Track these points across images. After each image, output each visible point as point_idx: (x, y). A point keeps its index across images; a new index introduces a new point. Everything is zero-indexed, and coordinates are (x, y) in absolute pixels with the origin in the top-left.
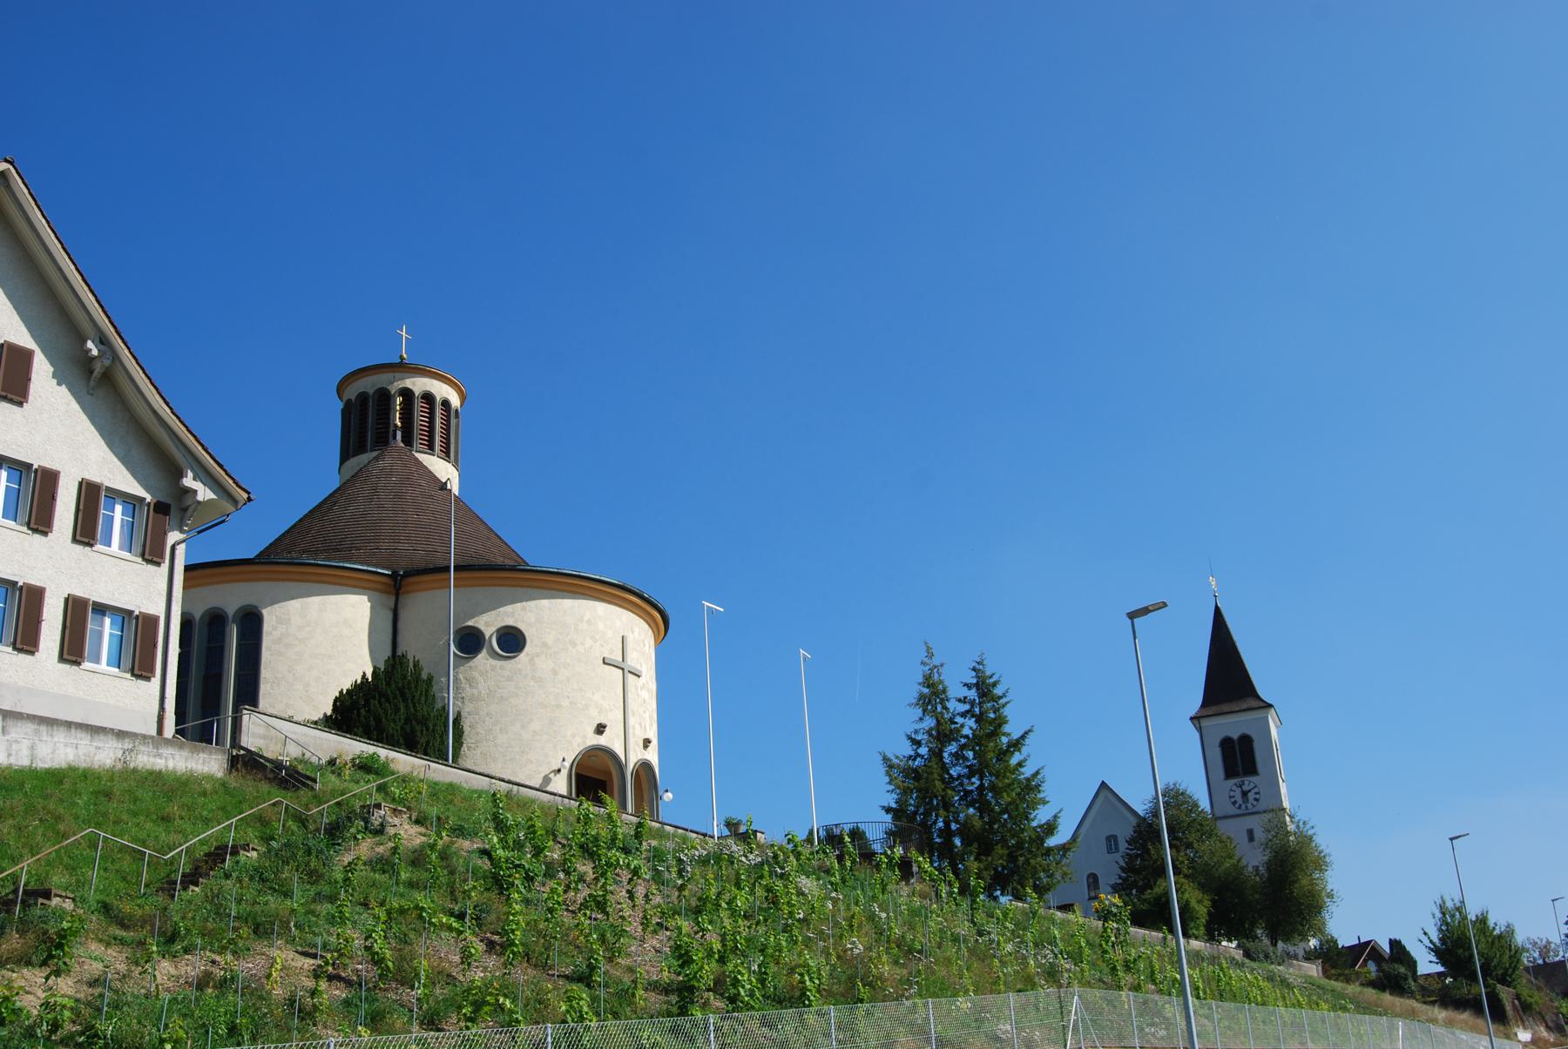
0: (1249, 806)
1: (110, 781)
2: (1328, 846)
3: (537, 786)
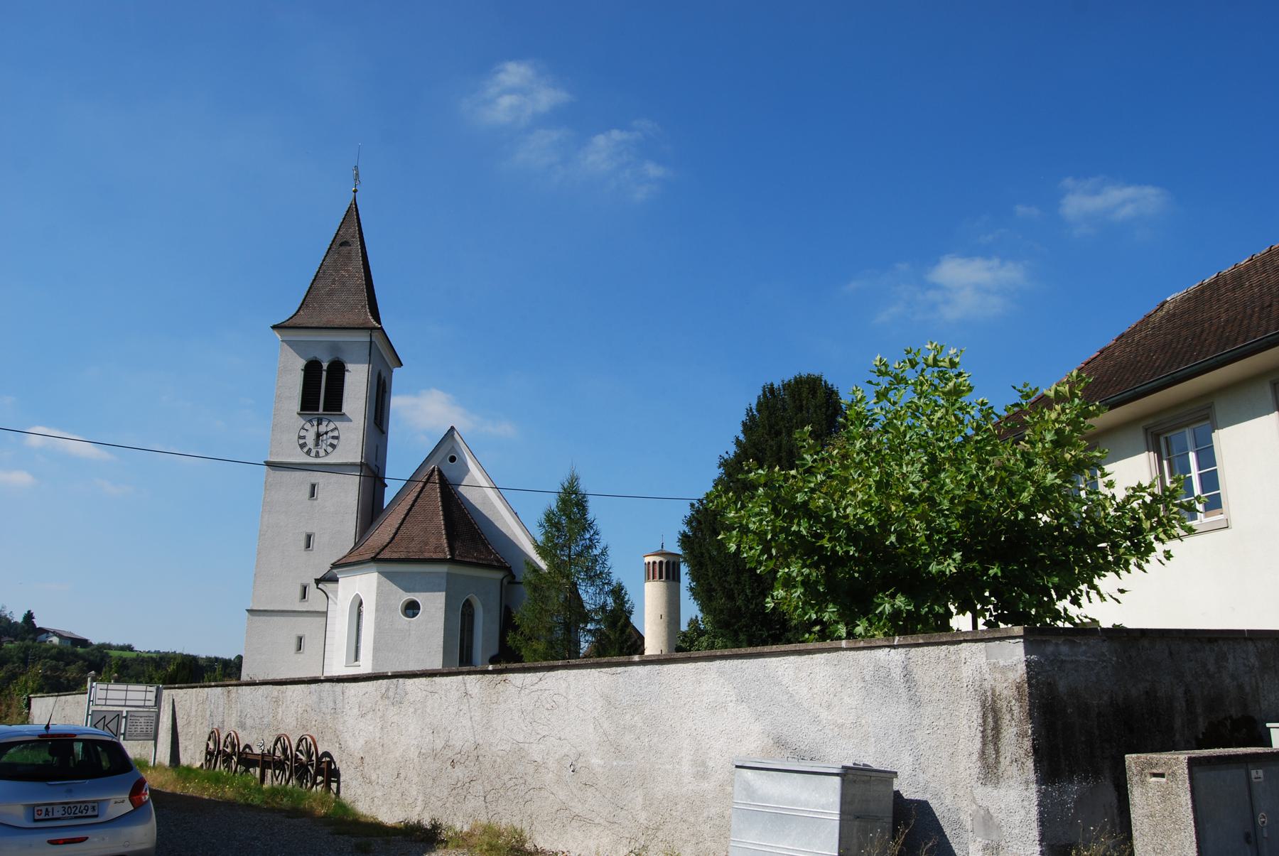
0: (322, 453)
2: (727, 453)
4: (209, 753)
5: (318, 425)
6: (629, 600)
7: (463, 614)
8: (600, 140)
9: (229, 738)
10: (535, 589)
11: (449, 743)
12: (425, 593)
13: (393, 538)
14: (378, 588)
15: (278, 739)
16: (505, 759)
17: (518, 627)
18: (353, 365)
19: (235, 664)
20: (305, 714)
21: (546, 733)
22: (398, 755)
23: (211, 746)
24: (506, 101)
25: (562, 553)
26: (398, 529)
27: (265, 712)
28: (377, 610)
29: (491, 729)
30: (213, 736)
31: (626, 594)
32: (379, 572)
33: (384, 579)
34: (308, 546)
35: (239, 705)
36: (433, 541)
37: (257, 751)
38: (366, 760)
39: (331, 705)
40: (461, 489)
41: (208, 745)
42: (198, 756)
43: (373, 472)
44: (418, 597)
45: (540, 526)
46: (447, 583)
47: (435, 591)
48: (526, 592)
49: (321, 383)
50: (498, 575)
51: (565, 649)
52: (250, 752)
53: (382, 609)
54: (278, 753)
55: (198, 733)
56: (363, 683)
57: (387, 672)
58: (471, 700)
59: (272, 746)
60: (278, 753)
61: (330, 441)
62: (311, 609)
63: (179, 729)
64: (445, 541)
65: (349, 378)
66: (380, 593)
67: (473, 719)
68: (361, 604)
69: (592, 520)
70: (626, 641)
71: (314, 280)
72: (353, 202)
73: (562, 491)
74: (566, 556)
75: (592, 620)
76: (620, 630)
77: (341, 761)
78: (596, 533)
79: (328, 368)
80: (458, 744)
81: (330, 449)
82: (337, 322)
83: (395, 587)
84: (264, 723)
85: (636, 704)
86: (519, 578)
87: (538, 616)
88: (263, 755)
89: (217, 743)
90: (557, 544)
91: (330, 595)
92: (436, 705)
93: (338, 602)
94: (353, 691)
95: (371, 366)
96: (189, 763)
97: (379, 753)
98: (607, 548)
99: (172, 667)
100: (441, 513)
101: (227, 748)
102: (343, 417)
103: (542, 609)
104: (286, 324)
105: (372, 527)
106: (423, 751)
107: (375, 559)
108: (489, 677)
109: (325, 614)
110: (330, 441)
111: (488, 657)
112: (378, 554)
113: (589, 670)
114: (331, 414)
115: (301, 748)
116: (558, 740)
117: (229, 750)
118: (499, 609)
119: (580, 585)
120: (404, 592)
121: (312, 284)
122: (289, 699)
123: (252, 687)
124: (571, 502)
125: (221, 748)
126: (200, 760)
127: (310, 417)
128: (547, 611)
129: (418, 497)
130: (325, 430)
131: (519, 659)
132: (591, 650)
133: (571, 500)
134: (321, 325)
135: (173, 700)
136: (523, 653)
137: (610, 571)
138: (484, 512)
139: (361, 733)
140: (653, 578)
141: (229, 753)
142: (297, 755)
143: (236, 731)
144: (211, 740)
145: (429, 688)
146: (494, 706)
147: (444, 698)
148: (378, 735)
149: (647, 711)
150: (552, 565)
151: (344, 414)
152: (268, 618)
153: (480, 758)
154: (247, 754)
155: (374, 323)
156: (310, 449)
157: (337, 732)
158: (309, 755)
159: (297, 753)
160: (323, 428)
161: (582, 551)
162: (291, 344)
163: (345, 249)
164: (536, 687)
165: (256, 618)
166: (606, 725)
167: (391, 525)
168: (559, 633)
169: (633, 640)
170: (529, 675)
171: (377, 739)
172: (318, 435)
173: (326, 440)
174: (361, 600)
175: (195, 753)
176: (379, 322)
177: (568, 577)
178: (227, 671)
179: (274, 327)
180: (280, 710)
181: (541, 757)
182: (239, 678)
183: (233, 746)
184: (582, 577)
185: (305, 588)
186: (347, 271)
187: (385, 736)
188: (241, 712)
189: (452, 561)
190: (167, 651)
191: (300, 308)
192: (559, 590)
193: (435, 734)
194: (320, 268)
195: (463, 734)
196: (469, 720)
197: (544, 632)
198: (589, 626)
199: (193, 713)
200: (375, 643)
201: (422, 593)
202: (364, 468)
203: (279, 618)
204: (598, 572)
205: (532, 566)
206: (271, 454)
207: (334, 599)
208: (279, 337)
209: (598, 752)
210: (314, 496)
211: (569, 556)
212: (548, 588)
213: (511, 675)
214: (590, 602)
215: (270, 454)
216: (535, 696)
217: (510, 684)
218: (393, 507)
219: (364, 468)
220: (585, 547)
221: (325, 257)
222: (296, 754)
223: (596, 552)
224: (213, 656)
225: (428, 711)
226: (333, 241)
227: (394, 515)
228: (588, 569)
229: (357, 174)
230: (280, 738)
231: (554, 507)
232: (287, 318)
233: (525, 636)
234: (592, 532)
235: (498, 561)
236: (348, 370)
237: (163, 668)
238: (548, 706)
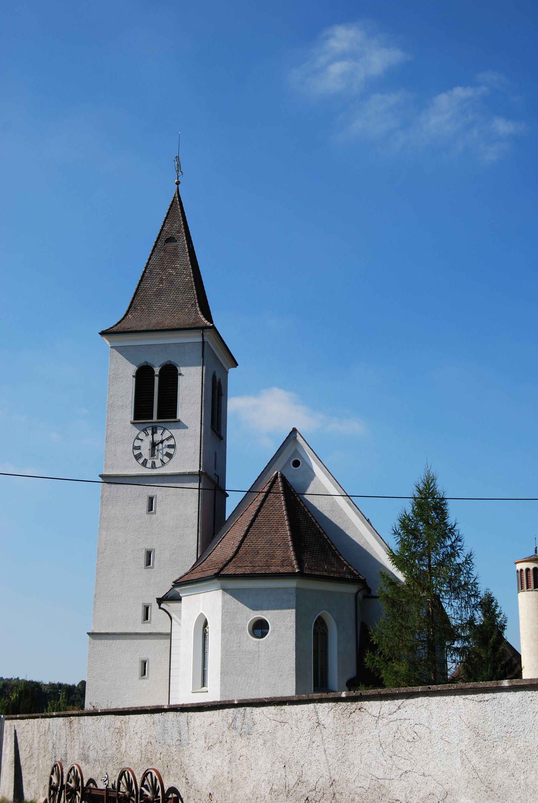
0: (158, 463)
1: (384, 578)
3: (170, 640)
4: (52, 788)
5: (153, 434)
6: (501, 614)
7: (315, 633)
8: (443, 100)
9: (72, 772)
10: (393, 603)
11: (303, 779)
12: (273, 611)
13: (237, 552)
14: (223, 607)
15: (122, 774)
16: (364, 797)
17: (376, 646)
18: (185, 368)
19: (79, 690)
20: (150, 747)
21: (408, 768)
22: (248, 791)
23: (55, 780)
24: (337, 68)
25: (421, 562)
26: (242, 541)
27: (109, 743)
28: (223, 631)
29: (347, 763)
30: (56, 769)
31: (497, 606)
33: (228, 596)
34: (148, 563)
35: (81, 737)
36: (279, 554)
37: (101, 786)
38: (215, 797)
39: (176, 736)
40: (306, 496)
41: (51, 779)
42: (41, 791)
43: (212, 481)
44: (266, 615)
45: (395, 533)
46: (296, 599)
47: (284, 609)
48: (383, 607)
50: (352, 589)
51: (429, 670)
52: (94, 787)
53: (229, 629)
54: (123, 789)
55: (41, 766)
56: (208, 712)
57: (233, 700)
58: (324, 731)
59: (117, 781)
60: (123, 789)
61: (166, 450)
62: (155, 631)
63: (22, 762)
64: (292, 553)
65: (182, 382)
66: (225, 612)
67: (327, 752)
68: (206, 624)
69: (453, 524)
70: (500, 660)
71: (141, 281)
72: (177, 196)
73: (417, 495)
74: (425, 566)
75: (459, 637)
76: (492, 647)
77: (188, 798)
78: (458, 539)
79: (160, 372)
80: (312, 780)
81: (166, 459)
82: (168, 323)
83: (241, 605)
84: (108, 755)
85: (508, 735)
86: (376, 592)
87: (398, 633)
88: (107, 790)
89: (60, 777)
90: (415, 553)
91: (173, 615)
92: (286, 736)
93: (182, 622)
94: (198, 721)
96: (33, 798)
97: (228, 789)
98: (471, 555)
99: (14, 696)
100: (287, 523)
101: (71, 782)
102: (178, 424)
103: (402, 625)
104: (119, 328)
105: (214, 541)
106: (275, 787)
107: (218, 576)
108: (343, 705)
109: (169, 636)
110: (166, 450)
111: (345, 681)
112: (222, 569)
113: (452, 697)
114: (170, 422)
115: (146, 783)
116: (422, 777)
117: (72, 785)
118: (354, 627)
119: (443, 598)
120: (251, 610)
121: (139, 285)
122: (132, 730)
123: (93, 717)
124: (428, 505)
125: (65, 783)
126: (44, 796)
127: (144, 426)
128: (407, 628)
129: (261, 506)
130: (160, 439)
131: (379, 683)
132: (459, 671)
133: (428, 504)
134: (150, 328)
135: (15, 731)
136: (382, 676)
137: (477, 581)
138: (333, 520)
139: (208, 767)
140: (528, 588)
141: (72, 788)
142: (142, 791)
143: (79, 764)
144: (55, 774)
145: (278, 718)
146: (350, 738)
147: (295, 729)
148: (226, 769)
149: (521, 744)
150: (409, 576)
151: (179, 421)
152: (111, 642)
153: (337, 796)
154: (91, 789)
155: (206, 321)
156: (145, 459)
157: (183, 765)
158: (155, 791)
159: (143, 788)
160: (158, 437)
161: (443, 559)
162: (121, 350)
163: (171, 245)
164: (395, 716)
165: (98, 642)
166: (475, 760)
167: (234, 538)
168: (423, 653)
169: (508, 658)
170: (386, 702)
171: (225, 774)
172: (154, 445)
173: (163, 448)
174: (206, 620)
175: (38, 787)
176: (211, 321)
177: (428, 589)
178: (71, 698)
179: (103, 333)
180: (123, 742)
181: (404, 796)
182: (83, 707)
183: (77, 780)
184: (445, 589)
185: (147, 608)
186: (175, 268)
187: (234, 770)
188: (84, 743)
189: (301, 575)
190: (9, 677)
191: (128, 312)
192: (420, 605)
193: (287, 769)
194: (146, 268)
195: (317, 769)
196: (323, 752)
197: (404, 652)
198: (456, 645)
199: (36, 745)
200: (222, 667)
201: (270, 611)
203: (121, 641)
204: (463, 583)
205: (388, 578)
206: (106, 467)
207: (178, 619)
208: (108, 343)
209: (468, 790)
210: (152, 510)
211: (429, 566)
212: (408, 603)
213: (367, 702)
214: (456, 617)
215: (105, 467)
216: (394, 726)
217: (366, 713)
218: (236, 518)
220: (446, 555)
221: (151, 255)
222: (141, 789)
223: (459, 560)
224: (56, 683)
225: (279, 743)
226: (158, 238)
227: (236, 527)
228: (451, 580)
229: (179, 165)
230: (124, 772)
231: (409, 512)
232: (116, 323)
233: (384, 656)
234: (453, 539)
235: (352, 573)
236: (181, 374)
237: (6, 696)
238: (409, 738)
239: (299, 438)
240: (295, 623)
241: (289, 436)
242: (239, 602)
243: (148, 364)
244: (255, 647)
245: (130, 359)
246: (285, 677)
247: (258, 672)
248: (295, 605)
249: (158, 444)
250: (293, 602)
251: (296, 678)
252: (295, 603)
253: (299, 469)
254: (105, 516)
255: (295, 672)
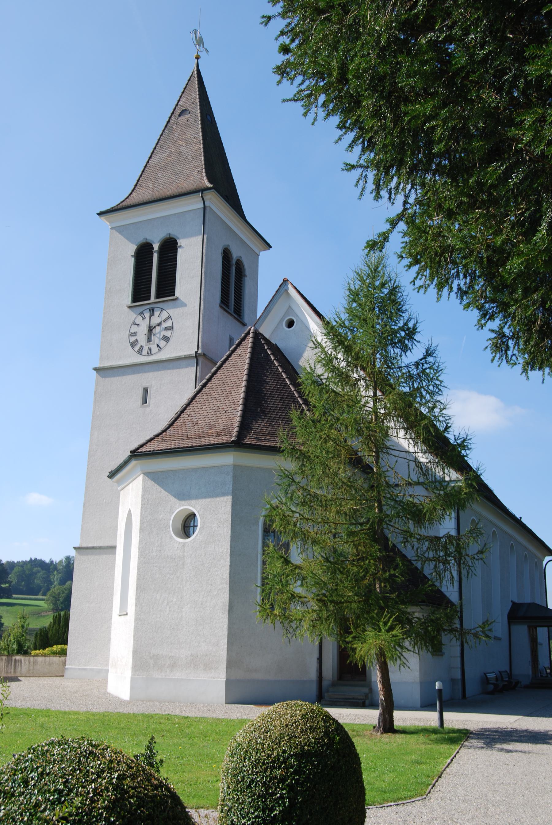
0: (154, 349)
32: (144, 474)
33: (150, 483)
46: (234, 480)
47: (217, 496)
49: (151, 269)
81: (162, 343)
83: (164, 493)
95: (205, 236)
104: (119, 207)
114: (167, 301)
127: (141, 309)
151: (177, 299)
156: (142, 346)
160: (155, 320)
172: (150, 329)
173: (160, 333)
202: (201, 360)
219: (201, 360)
236: (180, 246)
239: (292, 291)
240: (230, 515)
241: (279, 289)
242: (162, 489)
243: (147, 241)
244: (179, 551)
245: (129, 238)
246: (215, 593)
247: (182, 586)
248: (231, 489)
249: (155, 327)
250: (229, 487)
251: (230, 594)
252: (231, 486)
253: (293, 330)
254: (98, 413)
255: (228, 585)
